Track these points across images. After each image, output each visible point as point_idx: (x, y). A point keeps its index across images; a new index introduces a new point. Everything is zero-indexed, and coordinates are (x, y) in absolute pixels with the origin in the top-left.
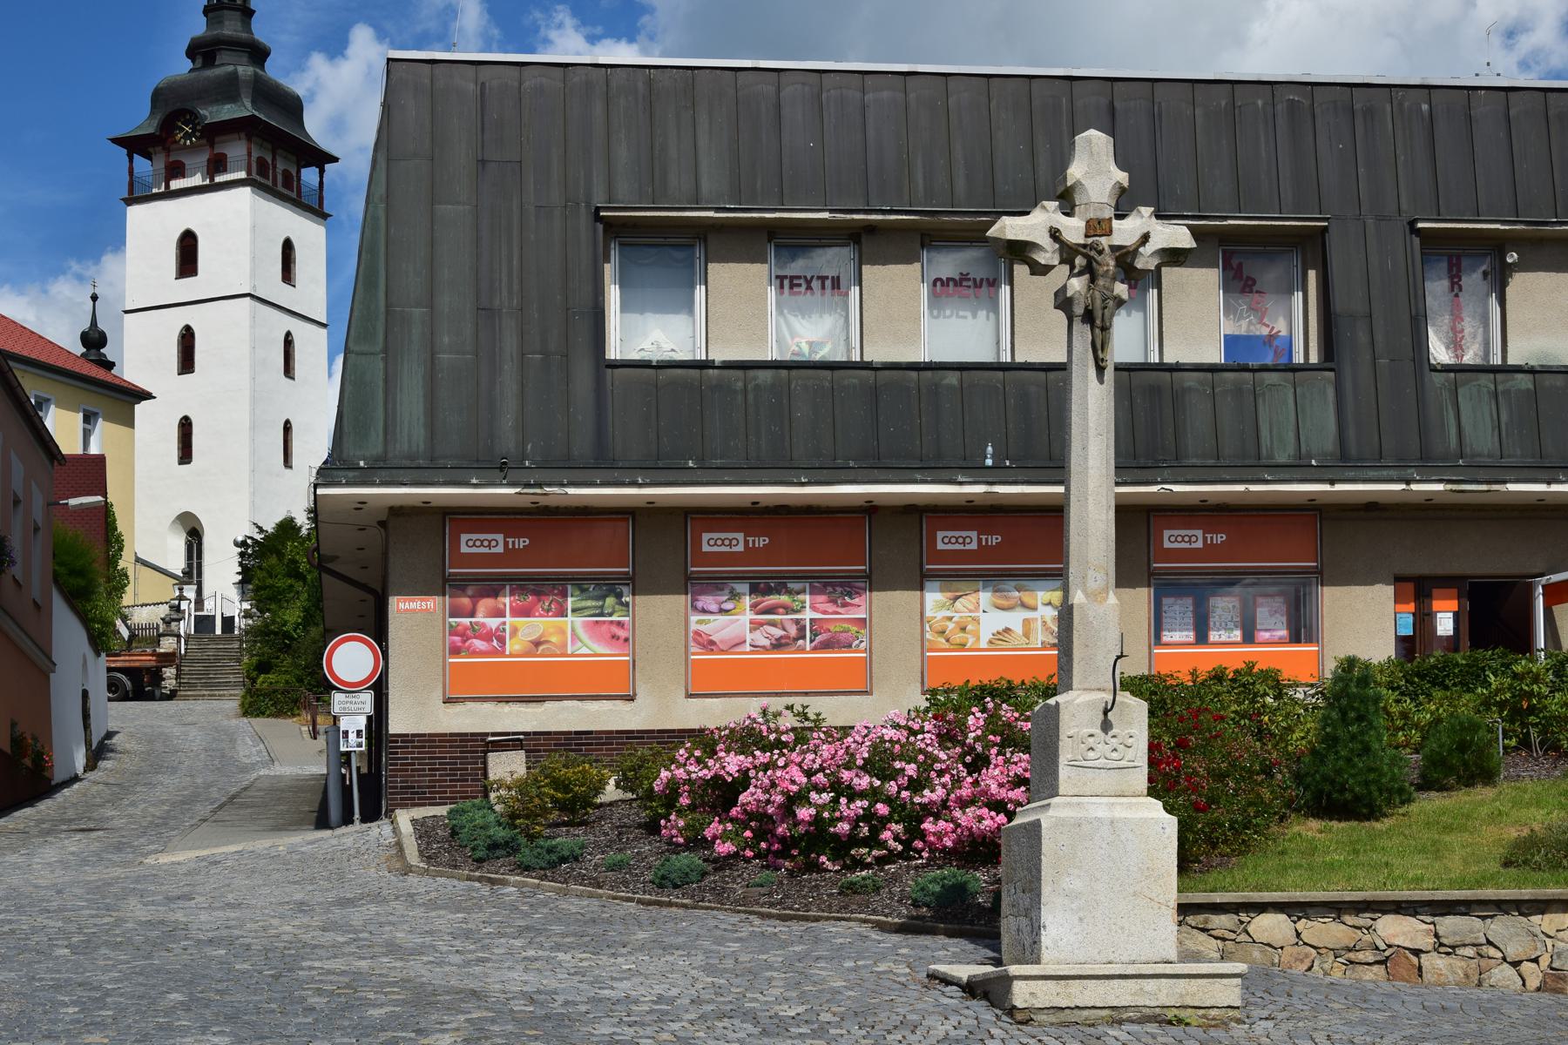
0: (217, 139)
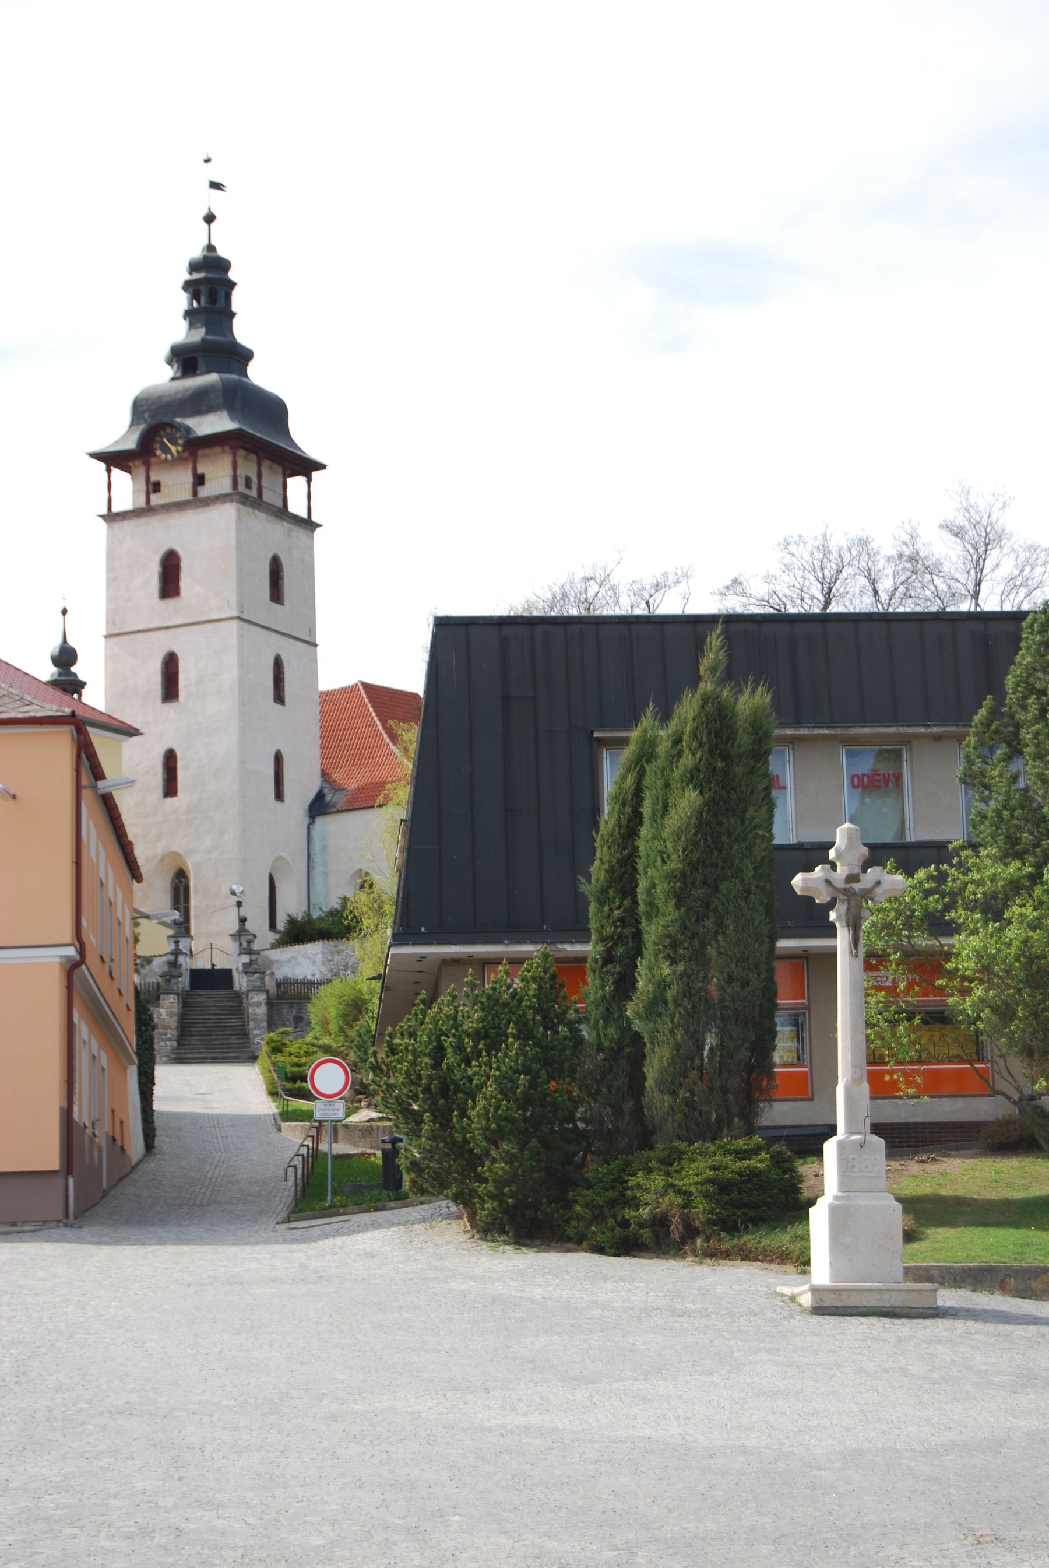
0: (200, 452)
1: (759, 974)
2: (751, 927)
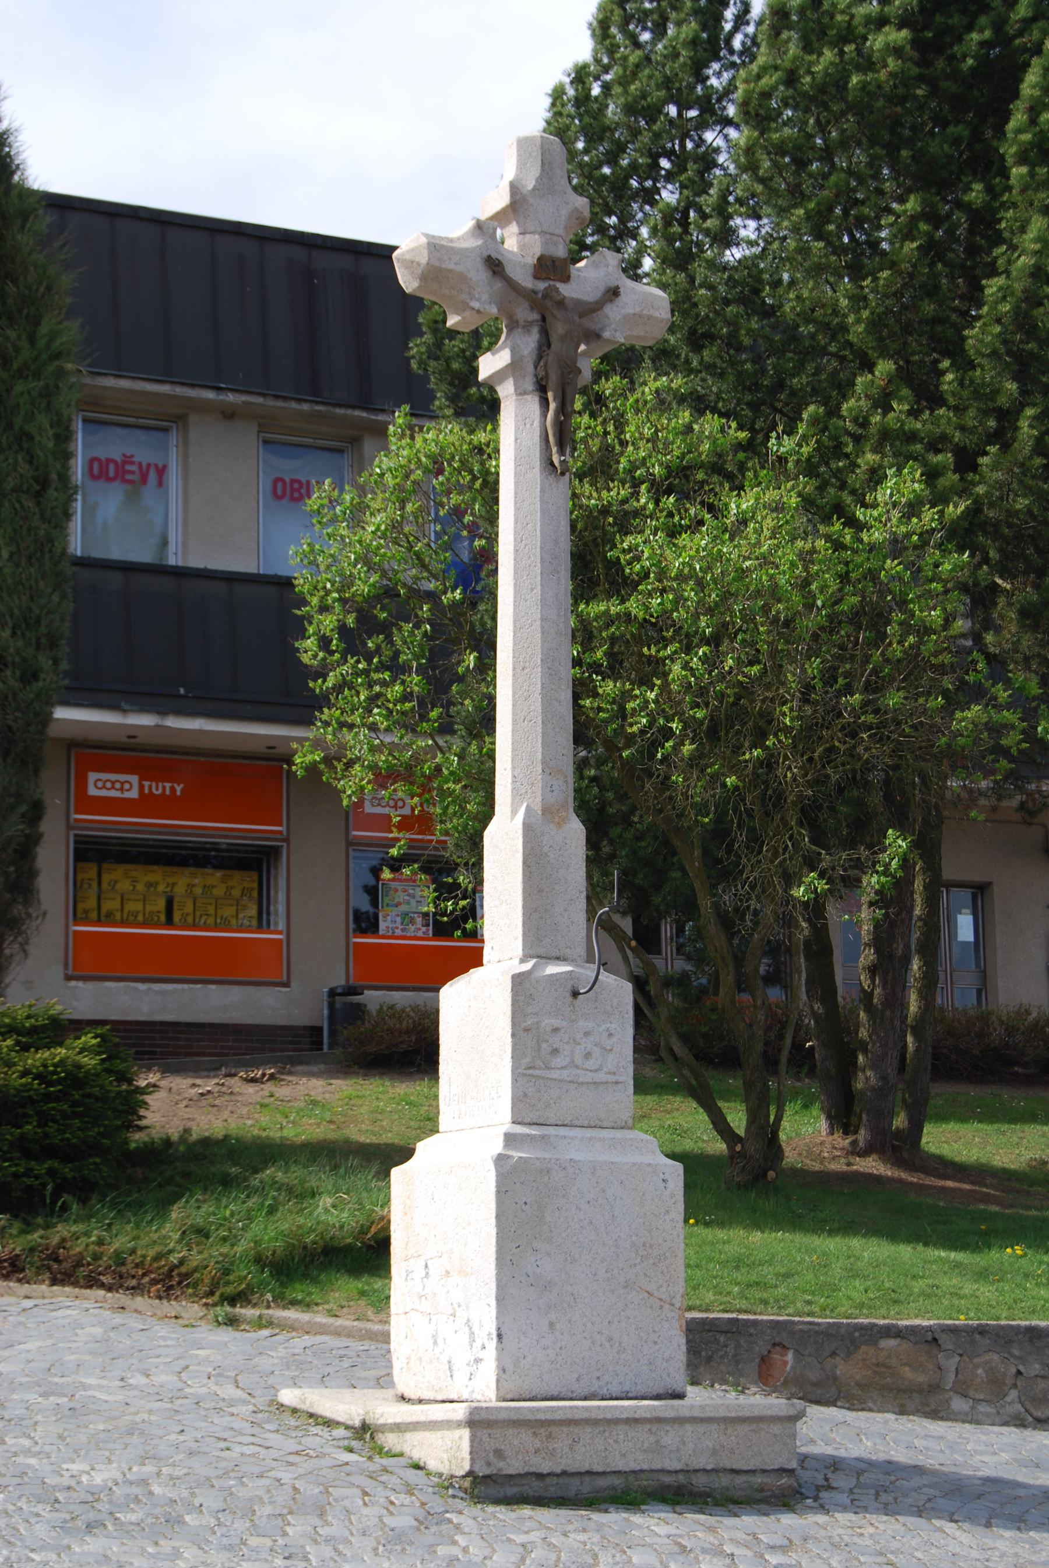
1: (56, 662)
2: (47, 556)
